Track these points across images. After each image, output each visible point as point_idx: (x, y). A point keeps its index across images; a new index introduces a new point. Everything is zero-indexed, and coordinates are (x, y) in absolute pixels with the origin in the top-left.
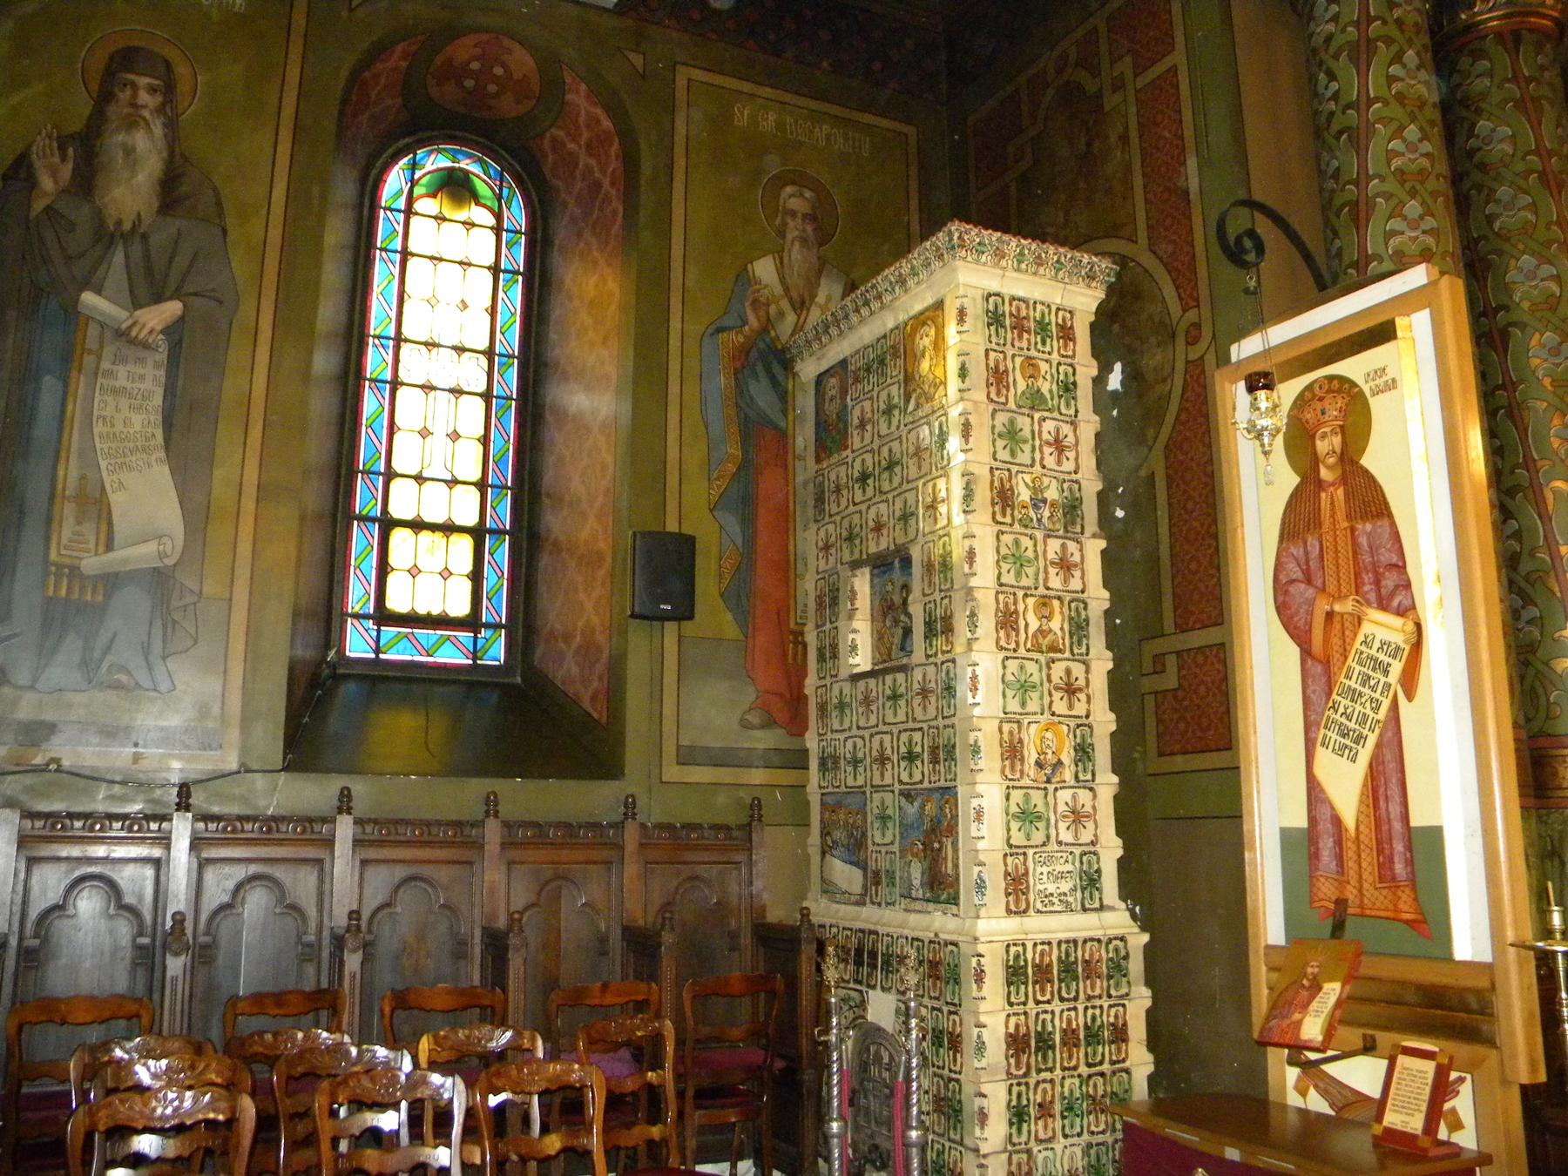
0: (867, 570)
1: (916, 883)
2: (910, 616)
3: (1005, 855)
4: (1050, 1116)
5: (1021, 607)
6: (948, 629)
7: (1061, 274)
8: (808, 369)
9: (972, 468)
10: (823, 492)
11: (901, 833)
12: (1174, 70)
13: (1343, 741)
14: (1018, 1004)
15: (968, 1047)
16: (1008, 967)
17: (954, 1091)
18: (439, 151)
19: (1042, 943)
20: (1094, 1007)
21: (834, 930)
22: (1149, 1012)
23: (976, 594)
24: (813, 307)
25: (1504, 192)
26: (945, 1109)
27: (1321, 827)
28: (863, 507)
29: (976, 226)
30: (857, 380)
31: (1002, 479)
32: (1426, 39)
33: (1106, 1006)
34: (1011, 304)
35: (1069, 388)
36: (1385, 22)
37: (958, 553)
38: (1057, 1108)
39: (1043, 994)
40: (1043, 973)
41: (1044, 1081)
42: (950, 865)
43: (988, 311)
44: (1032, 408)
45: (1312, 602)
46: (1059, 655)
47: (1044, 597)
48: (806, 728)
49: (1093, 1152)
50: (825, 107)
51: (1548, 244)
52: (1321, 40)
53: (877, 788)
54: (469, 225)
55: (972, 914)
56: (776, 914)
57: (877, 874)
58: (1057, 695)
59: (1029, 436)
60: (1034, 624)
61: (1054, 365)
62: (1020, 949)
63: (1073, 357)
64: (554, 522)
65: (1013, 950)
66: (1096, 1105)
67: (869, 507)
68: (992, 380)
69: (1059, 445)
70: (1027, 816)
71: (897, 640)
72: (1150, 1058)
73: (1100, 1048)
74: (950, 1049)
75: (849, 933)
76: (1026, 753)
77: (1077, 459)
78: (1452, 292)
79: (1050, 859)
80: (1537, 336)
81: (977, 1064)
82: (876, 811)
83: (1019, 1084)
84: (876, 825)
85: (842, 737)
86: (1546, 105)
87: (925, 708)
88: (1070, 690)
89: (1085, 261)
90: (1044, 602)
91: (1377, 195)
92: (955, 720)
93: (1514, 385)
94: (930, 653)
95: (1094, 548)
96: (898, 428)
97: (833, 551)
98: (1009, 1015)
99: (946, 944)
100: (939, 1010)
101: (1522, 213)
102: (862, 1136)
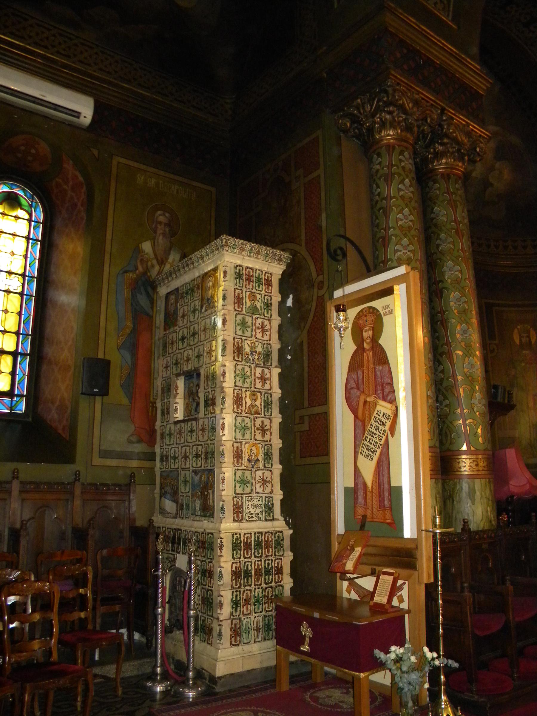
0: (183, 377)
1: (198, 509)
2: (199, 398)
3: (233, 498)
4: (249, 604)
5: (244, 395)
6: (214, 404)
7: (267, 258)
8: (163, 291)
9: (226, 338)
10: (166, 343)
11: (192, 488)
12: (319, 176)
13: (368, 452)
14: (237, 558)
15: (216, 576)
16: (233, 543)
17: (210, 595)
18: (4, 184)
19: (248, 534)
20: (269, 560)
21: (164, 529)
22: (291, 562)
23: (225, 390)
24: (167, 264)
25: (443, 235)
26: (206, 603)
27: (359, 487)
28: (182, 351)
29: (233, 237)
30: (182, 297)
31: (238, 343)
32: (413, 175)
33: (274, 559)
34: (246, 270)
35: (268, 306)
36: (398, 168)
37: (219, 372)
38: (252, 601)
39: (247, 554)
40: (248, 546)
41: (247, 590)
42: (211, 501)
43: (236, 273)
44: (253, 313)
45: (359, 397)
46: (259, 416)
47: (254, 391)
48: (155, 444)
49: (266, 619)
50: (177, 178)
51: (457, 257)
52: (375, 171)
53: (183, 469)
54: (17, 218)
55: (219, 521)
56: (140, 522)
57: (182, 505)
58: (257, 432)
59: (251, 325)
60: (249, 402)
61: (263, 296)
62: (238, 536)
63: (271, 293)
64: (49, 351)
65: (235, 536)
66: (269, 600)
67: (184, 351)
68: (236, 301)
69: (263, 329)
70: (243, 481)
71: (194, 407)
72: (291, 581)
73: (271, 577)
74: (209, 577)
75: (170, 530)
76: (244, 456)
77: (270, 335)
78: (415, 277)
79: (253, 499)
80: (453, 293)
81: (219, 583)
82: (183, 479)
83: (236, 591)
84: (183, 485)
85: (170, 447)
86: (459, 203)
87: (203, 436)
88: (263, 430)
89: (278, 253)
90: (254, 394)
91: (392, 235)
92: (215, 441)
93: (444, 312)
94: (206, 413)
95: (276, 372)
96: (198, 319)
97: (169, 369)
98: (233, 563)
99: (209, 533)
100: (205, 561)
101: (449, 245)
102: (173, 616)
